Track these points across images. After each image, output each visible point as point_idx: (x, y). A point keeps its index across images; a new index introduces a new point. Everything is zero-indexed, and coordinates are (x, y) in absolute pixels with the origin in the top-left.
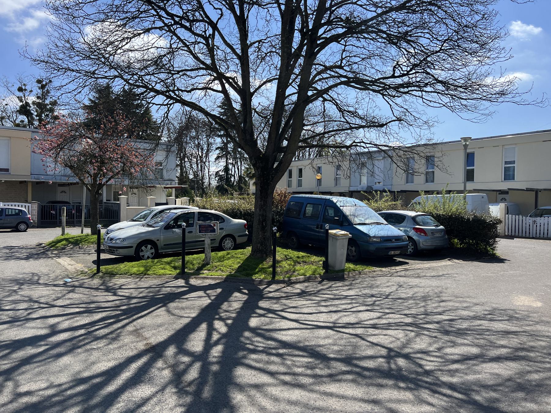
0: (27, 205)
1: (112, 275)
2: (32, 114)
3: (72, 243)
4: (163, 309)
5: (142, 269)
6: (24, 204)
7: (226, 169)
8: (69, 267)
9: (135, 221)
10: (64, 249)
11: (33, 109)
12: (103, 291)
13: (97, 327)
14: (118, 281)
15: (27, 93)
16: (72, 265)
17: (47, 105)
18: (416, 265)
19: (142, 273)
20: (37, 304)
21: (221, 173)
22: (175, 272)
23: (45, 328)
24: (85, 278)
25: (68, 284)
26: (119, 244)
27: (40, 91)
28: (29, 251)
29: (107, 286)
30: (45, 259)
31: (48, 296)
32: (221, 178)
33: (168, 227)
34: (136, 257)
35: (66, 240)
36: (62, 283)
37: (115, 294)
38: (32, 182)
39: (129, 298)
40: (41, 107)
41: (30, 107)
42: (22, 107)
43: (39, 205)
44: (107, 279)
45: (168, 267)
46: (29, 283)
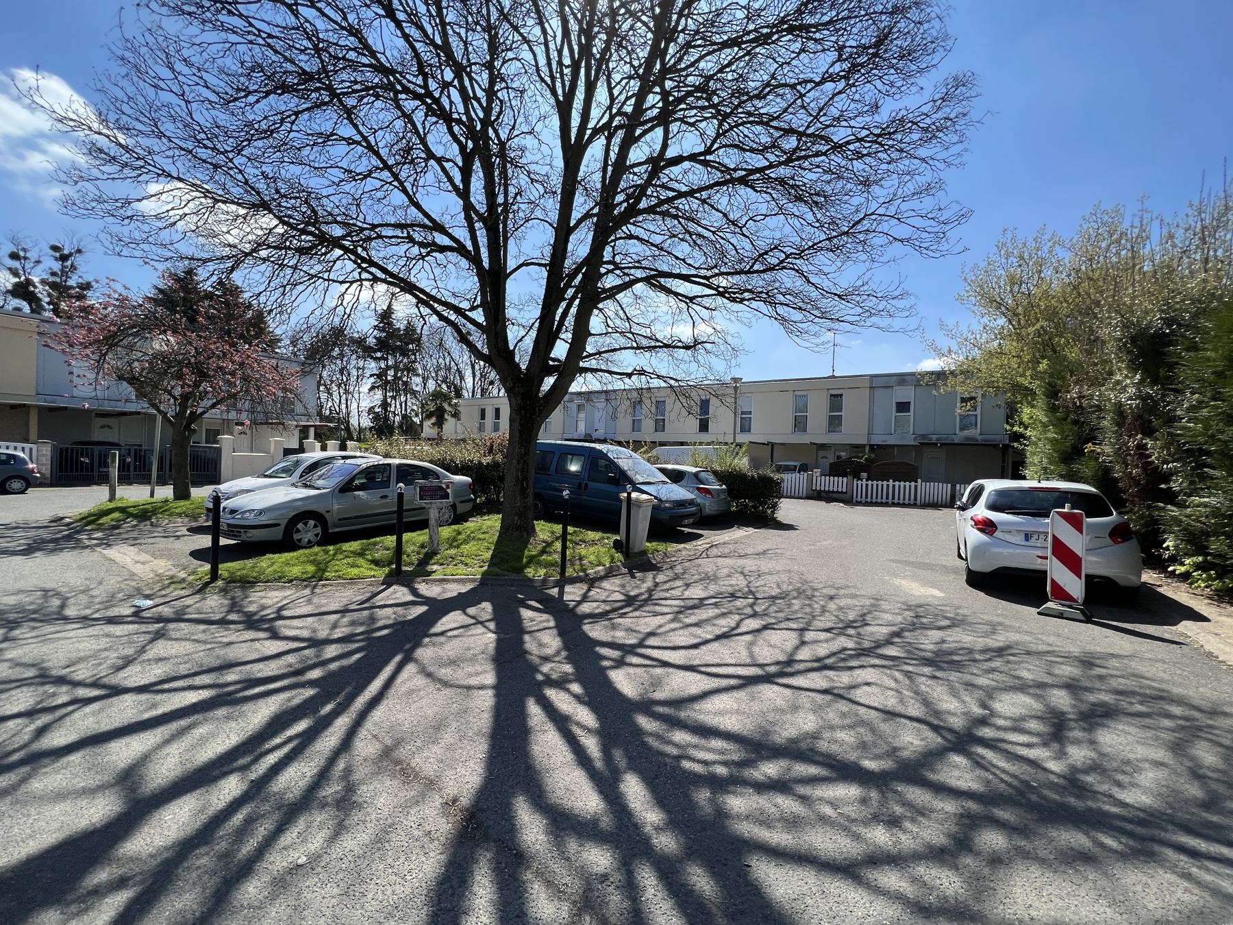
0: (27, 446)
1: (247, 583)
2: (40, 300)
3: (135, 516)
4: (410, 668)
5: (311, 568)
6: (20, 445)
7: (385, 405)
8: (138, 569)
9: (270, 476)
10: (117, 527)
11: (42, 292)
12: (240, 627)
13: (272, 759)
14: (265, 599)
15: (28, 265)
16: (143, 563)
17: (71, 287)
18: (712, 537)
19: (313, 577)
20: (64, 688)
21: (377, 410)
22: (381, 573)
23: (101, 788)
24: (183, 593)
25: (145, 614)
26: (251, 519)
27: (57, 266)
28: (32, 533)
29: (245, 613)
30: (75, 552)
31: (95, 655)
32: (377, 417)
33: (347, 487)
34: (287, 543)
35: (122, 510)
36: (129, 611)
37: (275, 636)
38: (40, 408)
39: (315, 643)
40: (59, 288)
41: (35, 287)
42: (16, 285)
43: (54, 448)
44: (238, 593)
45: (361, 561)
46: (34, 620)
